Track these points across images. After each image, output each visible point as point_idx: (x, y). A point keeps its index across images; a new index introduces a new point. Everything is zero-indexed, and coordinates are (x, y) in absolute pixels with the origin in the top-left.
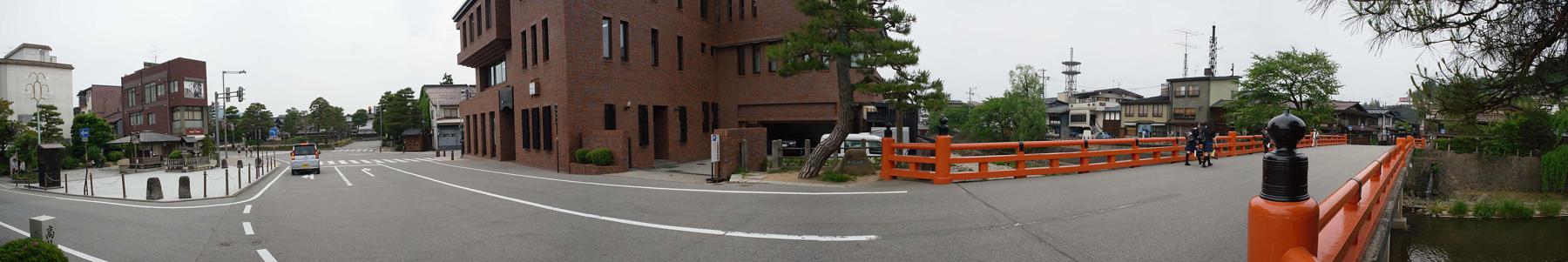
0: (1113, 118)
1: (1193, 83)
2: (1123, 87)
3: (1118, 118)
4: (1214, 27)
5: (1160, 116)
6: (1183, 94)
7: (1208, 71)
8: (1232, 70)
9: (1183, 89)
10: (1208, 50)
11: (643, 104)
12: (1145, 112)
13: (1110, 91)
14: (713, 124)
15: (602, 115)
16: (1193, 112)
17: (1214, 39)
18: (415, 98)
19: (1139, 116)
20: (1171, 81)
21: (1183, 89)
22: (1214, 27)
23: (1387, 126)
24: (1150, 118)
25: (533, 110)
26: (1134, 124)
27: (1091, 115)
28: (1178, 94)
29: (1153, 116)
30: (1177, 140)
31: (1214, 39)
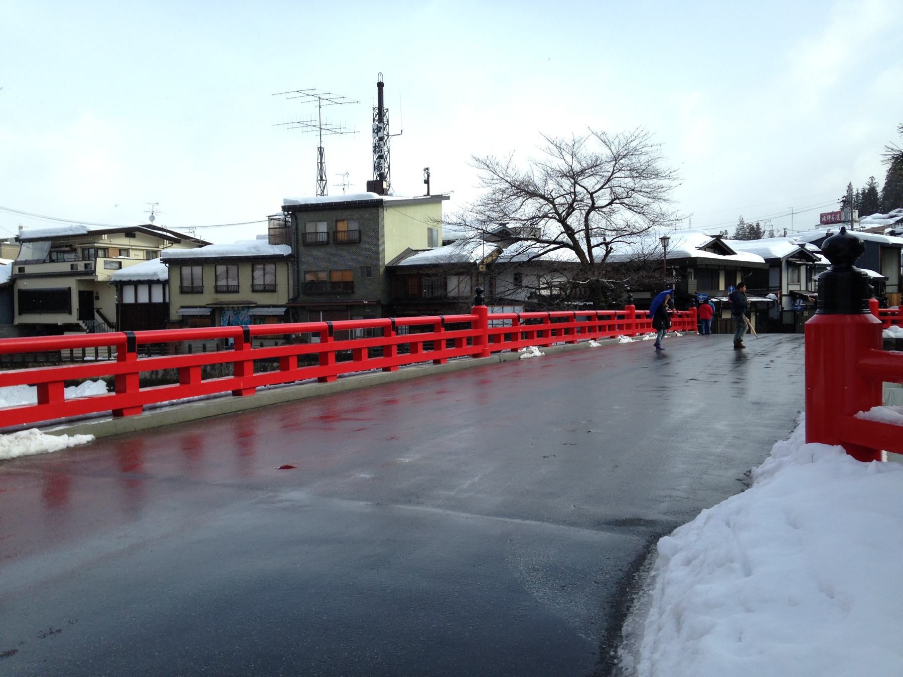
0: (143, 298)
1: (346, 214)
2: (167, 221)
3: (158, 298)
4: (380, 85)
5: (199, 291)
6: (323, 238)
7: (375, 186)
8: (427, 182)
9: (323, 227)
10: (369, 140)
11: (889, 279)
12: (197, 283)
13: (130, 232)
14: (48, 362)
15: (324, 351)
16: (348, 277)
17: (381, 113)
18: (836, 234)
19: (217, 290)
20: (292, 210)
21: (323, 227)
22: (380, 85)
23: (794, 288)
24: (245, 295)
25: (676, 325)
26: (206, 312)
27: (81, 293)
28: (310, 239)
29: (254, 291)
30: (247, 333)
31: (381, 113)
